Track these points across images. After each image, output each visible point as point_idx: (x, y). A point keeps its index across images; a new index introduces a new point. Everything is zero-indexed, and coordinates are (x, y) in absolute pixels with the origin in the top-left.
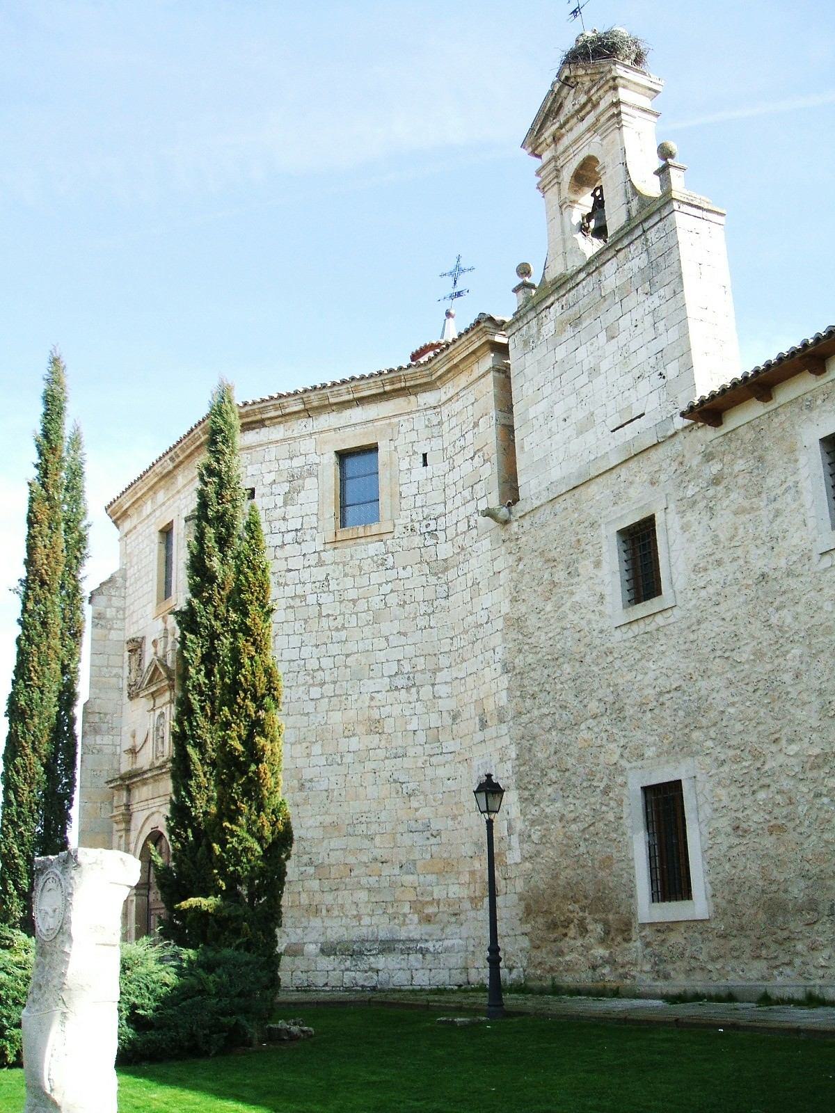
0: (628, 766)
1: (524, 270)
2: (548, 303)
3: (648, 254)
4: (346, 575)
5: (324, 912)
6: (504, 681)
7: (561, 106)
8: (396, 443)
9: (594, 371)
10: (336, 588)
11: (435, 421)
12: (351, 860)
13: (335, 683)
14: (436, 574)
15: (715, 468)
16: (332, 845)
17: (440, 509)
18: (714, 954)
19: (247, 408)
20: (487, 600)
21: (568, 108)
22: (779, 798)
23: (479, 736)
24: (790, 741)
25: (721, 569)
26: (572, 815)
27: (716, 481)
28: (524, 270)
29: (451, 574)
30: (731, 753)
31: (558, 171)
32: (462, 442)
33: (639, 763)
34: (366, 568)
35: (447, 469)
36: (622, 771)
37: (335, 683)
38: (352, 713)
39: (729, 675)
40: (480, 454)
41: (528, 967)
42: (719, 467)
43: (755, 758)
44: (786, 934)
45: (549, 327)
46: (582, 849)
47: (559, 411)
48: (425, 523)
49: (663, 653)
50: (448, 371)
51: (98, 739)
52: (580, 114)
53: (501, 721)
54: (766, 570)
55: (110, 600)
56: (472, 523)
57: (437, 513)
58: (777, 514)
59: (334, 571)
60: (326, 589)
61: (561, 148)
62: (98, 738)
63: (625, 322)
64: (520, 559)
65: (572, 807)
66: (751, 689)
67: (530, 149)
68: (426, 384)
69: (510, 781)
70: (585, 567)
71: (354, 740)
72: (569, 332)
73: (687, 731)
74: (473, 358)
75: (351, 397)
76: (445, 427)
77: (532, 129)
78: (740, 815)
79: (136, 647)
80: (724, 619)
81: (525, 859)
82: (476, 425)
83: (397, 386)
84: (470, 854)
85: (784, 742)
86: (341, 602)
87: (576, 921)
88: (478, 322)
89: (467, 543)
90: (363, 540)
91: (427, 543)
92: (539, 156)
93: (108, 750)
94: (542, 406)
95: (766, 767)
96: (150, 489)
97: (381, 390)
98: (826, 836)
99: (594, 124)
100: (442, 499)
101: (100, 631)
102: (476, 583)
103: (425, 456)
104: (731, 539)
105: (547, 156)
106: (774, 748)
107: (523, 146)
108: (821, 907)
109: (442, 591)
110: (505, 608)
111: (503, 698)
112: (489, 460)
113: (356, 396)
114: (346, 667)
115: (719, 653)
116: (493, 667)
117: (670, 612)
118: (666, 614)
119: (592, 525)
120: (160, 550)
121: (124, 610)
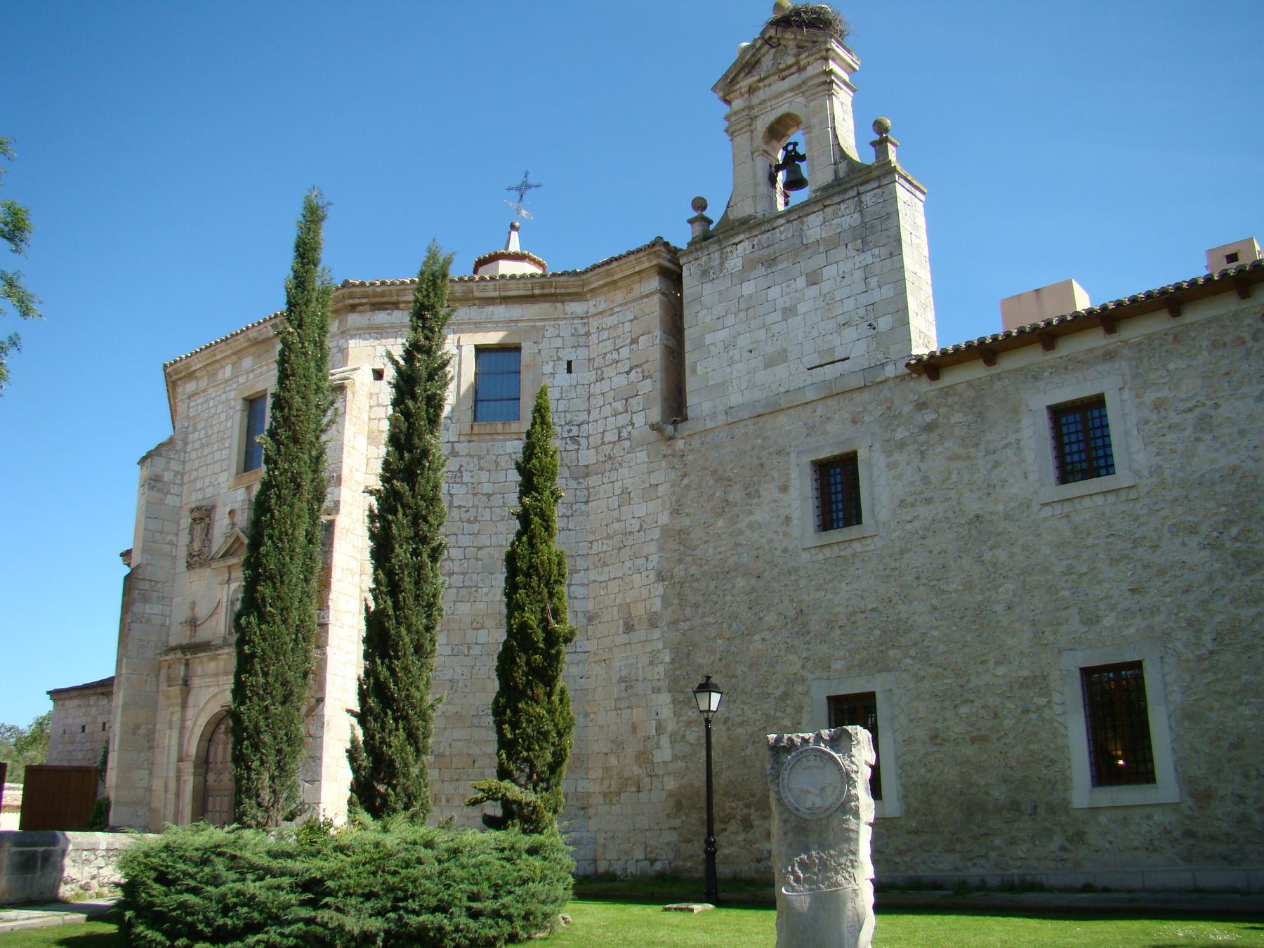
0: (810, 677)
1: (700, 204)
2: (736, 240)
3: (862, 215)
4: (481, 469)
5: (444, 801)
6: (659, 589)
7: (758, 61)
8: (541, 346)
9: (789, 312)
10: (470, 480)
11: (582, 331)
12: (475, 751)
13: (464, 574)
14: (576, 479)
15: (929, 417)
16: (455, 736)
17: (583, 417)
18: (902, 848)
19: (384, 288)
20: (641, 510)
21: (767, 62)
22: (983, 713)
23: (623, 639)
24: (999, 663)
25: (930, 507)
26: (740, 719)
27: (929, 428)
28: (700, 204)
29: (593, 481)
30: (931, 670)
31: (753, 119)
32: (615, 355)
33: (825, 675)
34: (503, 464)
35: (594, 378)
36: (803, 680)
37: (464, 574)
38: (481, 606)
39: (934, 602)
40: (639, 370)
41: (675, 858)
42: (934, 416)
43: (958, 676)
44: (982, 830)
45: (735, 263)
46: (749, 751)
47: (744, 341)
48: (567, 428)
49: (859, 576)
50: (604, 286)
51: (148, 608)
52: (782, 74)
53: (653, 625)
54: (980, 512)
55: (168, 463)
56: (624, 434)
57: (581, 419)
58: (996, 464)
59: (468, 463)
60: (458, 480)
61: (755, 100)
62: (147, 606)
63: (829, 272)
64: (685, 475)
65: (739, 712)
66: (957, 615)
67: (721, 94)
68: (576, 294)
69: (661, 683)
70: (769, 491)
71: (483, 633)
72: (761, 270)
73: (883, 648)
74: (637, 278)
75: (497, 294)
76: (594, 338)
77: (726, 76)
78: (939, 725)
79: (203, 515)
80: (931, 552)
81: (675, 757)
82: (634, 341)
83: (547, 291)
84: (605, 750)
85: (991, 664)
86: (474, 495)
87: (738, 817)
88: (653, 245)
89: (617, 452)
90: (501, 437)
91: (569, 448)
92: (728, 102)
93: (157, 620)
94: (721, 335)
95: (971, 685)
96: (235, 353)
97: (529, 293)
98: (1031, 747)
99: (799, 86)
100: (585, 406)
101: (155, 494)
102: (625, 492)
103: (569, 363)
104: (944, 481)
105: (738, 104)
106: (980, 668)
107: (714, 89)
108: (1023, 807)
109: (582, 495)
110: (664, 519)
111: (657, 605)
112: (650, 377)
113: (503, 294)
114: (477, 559)
115: (924, 581)
116: (645, 574)
117: (870, 540)
118: (864, 542)
119: (779, 453)
120: (242, 418)
121: (183, 474)
